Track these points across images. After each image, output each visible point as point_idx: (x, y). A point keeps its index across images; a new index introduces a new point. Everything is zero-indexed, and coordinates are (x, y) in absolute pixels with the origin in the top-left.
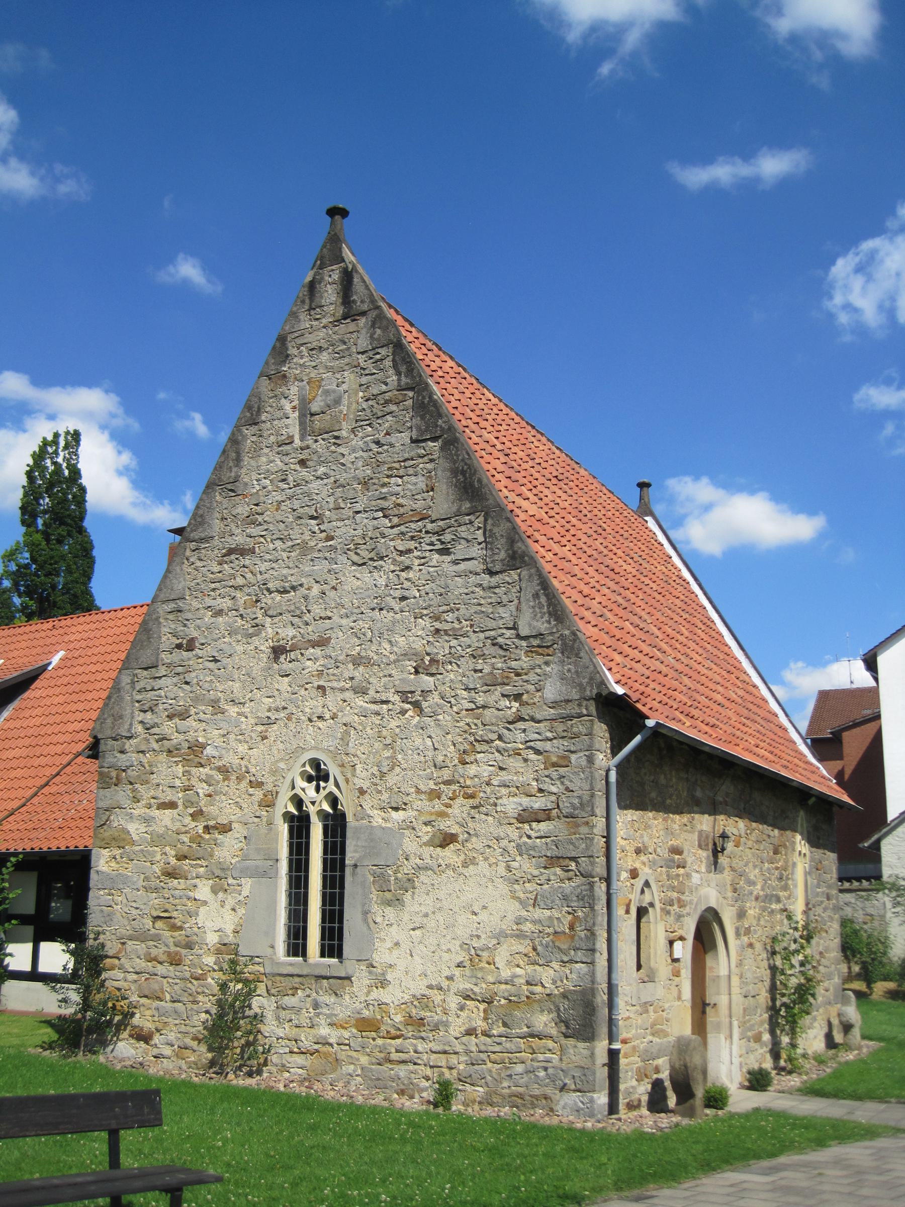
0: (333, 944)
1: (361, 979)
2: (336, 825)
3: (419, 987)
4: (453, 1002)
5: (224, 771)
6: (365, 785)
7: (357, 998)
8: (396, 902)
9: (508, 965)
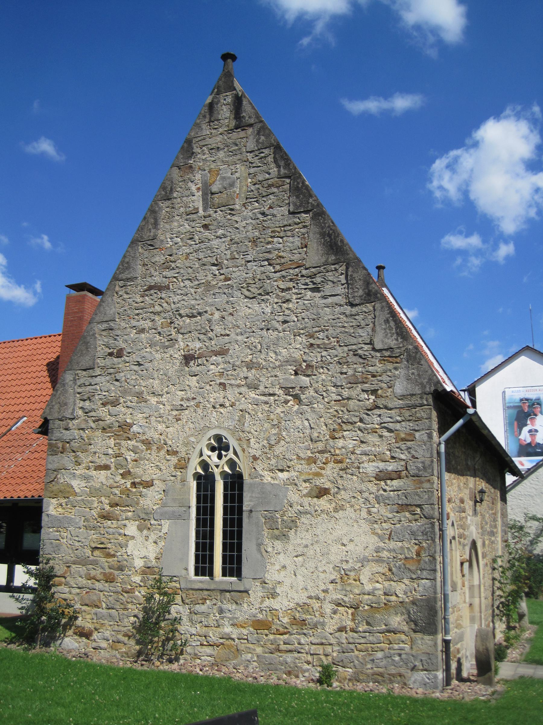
0: (233, 565)
1: (256, 593)
2: (235, 483)
3: (302, 598)
4: (328, 608)
5: (148, 443)
6: (258, 454)
7: (254, 604)
8: (284, 537)
9: (370, 581)
